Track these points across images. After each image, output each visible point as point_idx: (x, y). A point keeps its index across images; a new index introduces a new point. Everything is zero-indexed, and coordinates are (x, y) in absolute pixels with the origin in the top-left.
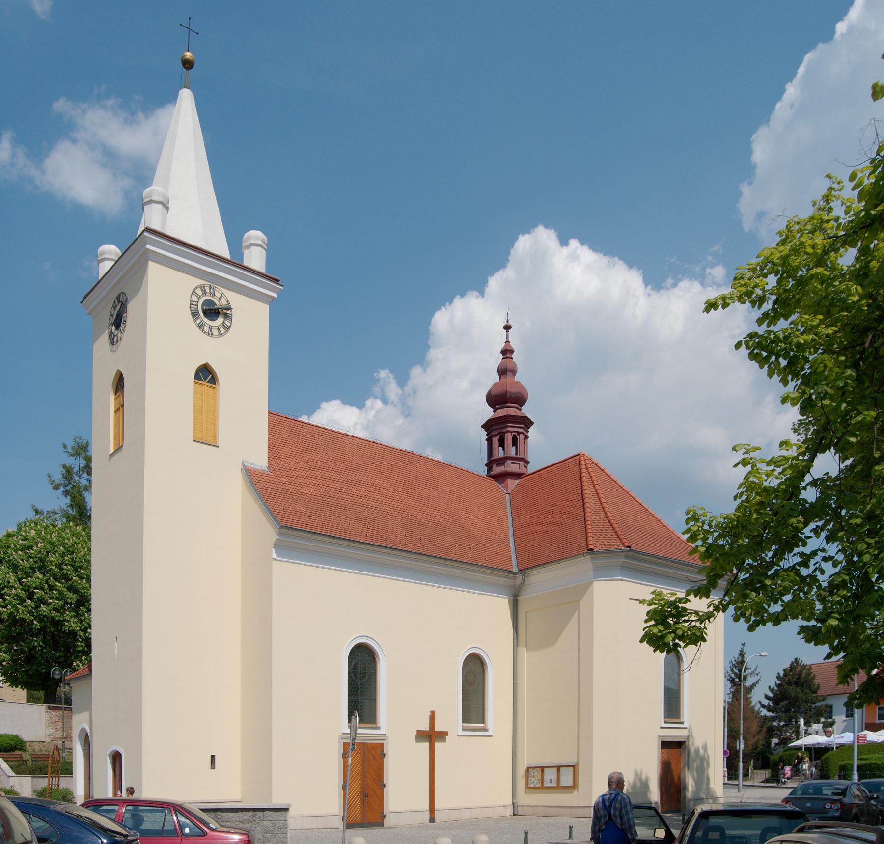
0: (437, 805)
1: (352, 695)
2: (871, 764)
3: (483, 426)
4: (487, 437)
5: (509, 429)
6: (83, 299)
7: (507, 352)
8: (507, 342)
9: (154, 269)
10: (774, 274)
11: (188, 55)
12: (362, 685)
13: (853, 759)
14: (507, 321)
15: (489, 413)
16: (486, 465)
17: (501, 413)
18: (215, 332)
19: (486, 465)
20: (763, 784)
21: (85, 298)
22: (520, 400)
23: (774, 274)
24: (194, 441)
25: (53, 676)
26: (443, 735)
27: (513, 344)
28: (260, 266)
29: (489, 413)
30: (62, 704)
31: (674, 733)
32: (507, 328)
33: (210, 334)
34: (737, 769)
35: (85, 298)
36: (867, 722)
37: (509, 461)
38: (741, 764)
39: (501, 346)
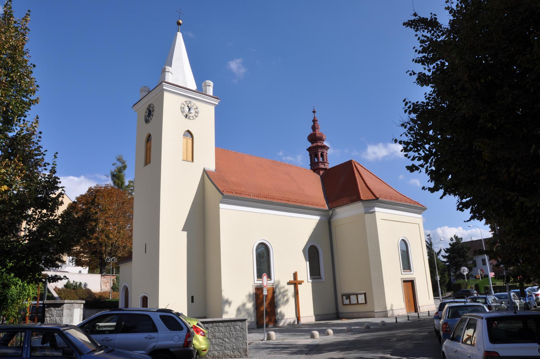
0: (301, 315)
1: (258, 266)
2: (289, 332)
3: (307, 150)
4: (309, 154)
5: (319, 151)
6: (133, 106)
7: (314, 121)
8: (314, 117)
9: (166, 94)
10: (421, 63)
11: (181, 22)
12: (263, 261)
13: (489, 284)
14: (314, 110)
15: (309, 145)
16: (310, 165)
17: (315, 145)
18: (191, 118)
19: (310, 165)
20: (105, 354)
21: (134, 105)
22: (321, 139)
23: (421, 63)
24: (183, 160)
25: (106, 261)
26: (301, 283)
27: (317, 118)
28: (211, 94)
29: (309, 145)
30: (110, 274)
31: (408, 276)
32: (314, 112)
34: (438, 291)
35: (134, 105)
36: (414, 312)
37: (320, 164)
38: (440, 289)
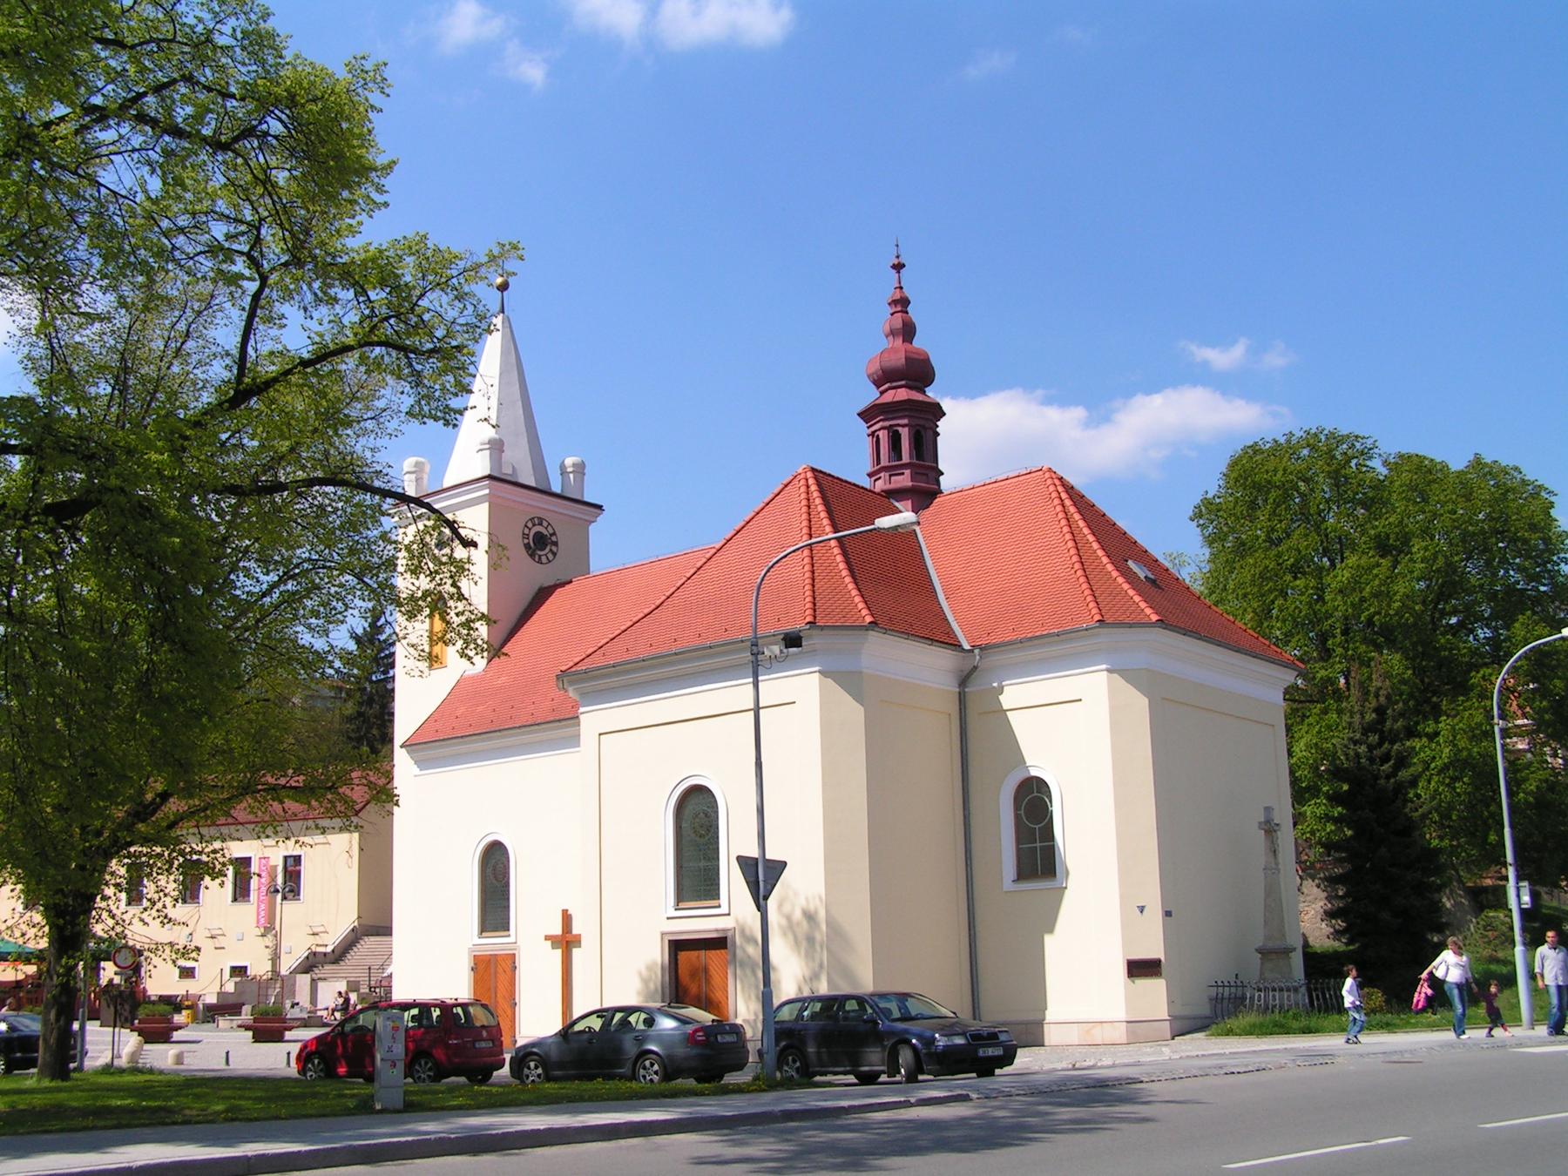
14: (898, 257)
18: (544, 559)
32: (898, 267)
33: (540, 562)
39: (890, 293)
